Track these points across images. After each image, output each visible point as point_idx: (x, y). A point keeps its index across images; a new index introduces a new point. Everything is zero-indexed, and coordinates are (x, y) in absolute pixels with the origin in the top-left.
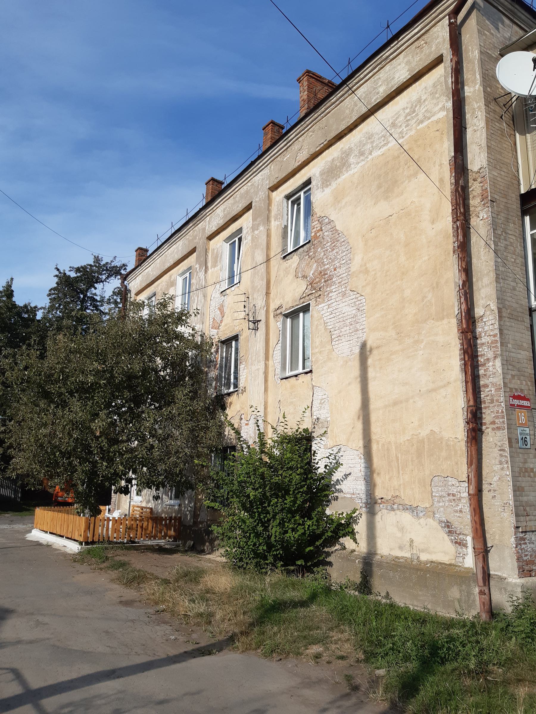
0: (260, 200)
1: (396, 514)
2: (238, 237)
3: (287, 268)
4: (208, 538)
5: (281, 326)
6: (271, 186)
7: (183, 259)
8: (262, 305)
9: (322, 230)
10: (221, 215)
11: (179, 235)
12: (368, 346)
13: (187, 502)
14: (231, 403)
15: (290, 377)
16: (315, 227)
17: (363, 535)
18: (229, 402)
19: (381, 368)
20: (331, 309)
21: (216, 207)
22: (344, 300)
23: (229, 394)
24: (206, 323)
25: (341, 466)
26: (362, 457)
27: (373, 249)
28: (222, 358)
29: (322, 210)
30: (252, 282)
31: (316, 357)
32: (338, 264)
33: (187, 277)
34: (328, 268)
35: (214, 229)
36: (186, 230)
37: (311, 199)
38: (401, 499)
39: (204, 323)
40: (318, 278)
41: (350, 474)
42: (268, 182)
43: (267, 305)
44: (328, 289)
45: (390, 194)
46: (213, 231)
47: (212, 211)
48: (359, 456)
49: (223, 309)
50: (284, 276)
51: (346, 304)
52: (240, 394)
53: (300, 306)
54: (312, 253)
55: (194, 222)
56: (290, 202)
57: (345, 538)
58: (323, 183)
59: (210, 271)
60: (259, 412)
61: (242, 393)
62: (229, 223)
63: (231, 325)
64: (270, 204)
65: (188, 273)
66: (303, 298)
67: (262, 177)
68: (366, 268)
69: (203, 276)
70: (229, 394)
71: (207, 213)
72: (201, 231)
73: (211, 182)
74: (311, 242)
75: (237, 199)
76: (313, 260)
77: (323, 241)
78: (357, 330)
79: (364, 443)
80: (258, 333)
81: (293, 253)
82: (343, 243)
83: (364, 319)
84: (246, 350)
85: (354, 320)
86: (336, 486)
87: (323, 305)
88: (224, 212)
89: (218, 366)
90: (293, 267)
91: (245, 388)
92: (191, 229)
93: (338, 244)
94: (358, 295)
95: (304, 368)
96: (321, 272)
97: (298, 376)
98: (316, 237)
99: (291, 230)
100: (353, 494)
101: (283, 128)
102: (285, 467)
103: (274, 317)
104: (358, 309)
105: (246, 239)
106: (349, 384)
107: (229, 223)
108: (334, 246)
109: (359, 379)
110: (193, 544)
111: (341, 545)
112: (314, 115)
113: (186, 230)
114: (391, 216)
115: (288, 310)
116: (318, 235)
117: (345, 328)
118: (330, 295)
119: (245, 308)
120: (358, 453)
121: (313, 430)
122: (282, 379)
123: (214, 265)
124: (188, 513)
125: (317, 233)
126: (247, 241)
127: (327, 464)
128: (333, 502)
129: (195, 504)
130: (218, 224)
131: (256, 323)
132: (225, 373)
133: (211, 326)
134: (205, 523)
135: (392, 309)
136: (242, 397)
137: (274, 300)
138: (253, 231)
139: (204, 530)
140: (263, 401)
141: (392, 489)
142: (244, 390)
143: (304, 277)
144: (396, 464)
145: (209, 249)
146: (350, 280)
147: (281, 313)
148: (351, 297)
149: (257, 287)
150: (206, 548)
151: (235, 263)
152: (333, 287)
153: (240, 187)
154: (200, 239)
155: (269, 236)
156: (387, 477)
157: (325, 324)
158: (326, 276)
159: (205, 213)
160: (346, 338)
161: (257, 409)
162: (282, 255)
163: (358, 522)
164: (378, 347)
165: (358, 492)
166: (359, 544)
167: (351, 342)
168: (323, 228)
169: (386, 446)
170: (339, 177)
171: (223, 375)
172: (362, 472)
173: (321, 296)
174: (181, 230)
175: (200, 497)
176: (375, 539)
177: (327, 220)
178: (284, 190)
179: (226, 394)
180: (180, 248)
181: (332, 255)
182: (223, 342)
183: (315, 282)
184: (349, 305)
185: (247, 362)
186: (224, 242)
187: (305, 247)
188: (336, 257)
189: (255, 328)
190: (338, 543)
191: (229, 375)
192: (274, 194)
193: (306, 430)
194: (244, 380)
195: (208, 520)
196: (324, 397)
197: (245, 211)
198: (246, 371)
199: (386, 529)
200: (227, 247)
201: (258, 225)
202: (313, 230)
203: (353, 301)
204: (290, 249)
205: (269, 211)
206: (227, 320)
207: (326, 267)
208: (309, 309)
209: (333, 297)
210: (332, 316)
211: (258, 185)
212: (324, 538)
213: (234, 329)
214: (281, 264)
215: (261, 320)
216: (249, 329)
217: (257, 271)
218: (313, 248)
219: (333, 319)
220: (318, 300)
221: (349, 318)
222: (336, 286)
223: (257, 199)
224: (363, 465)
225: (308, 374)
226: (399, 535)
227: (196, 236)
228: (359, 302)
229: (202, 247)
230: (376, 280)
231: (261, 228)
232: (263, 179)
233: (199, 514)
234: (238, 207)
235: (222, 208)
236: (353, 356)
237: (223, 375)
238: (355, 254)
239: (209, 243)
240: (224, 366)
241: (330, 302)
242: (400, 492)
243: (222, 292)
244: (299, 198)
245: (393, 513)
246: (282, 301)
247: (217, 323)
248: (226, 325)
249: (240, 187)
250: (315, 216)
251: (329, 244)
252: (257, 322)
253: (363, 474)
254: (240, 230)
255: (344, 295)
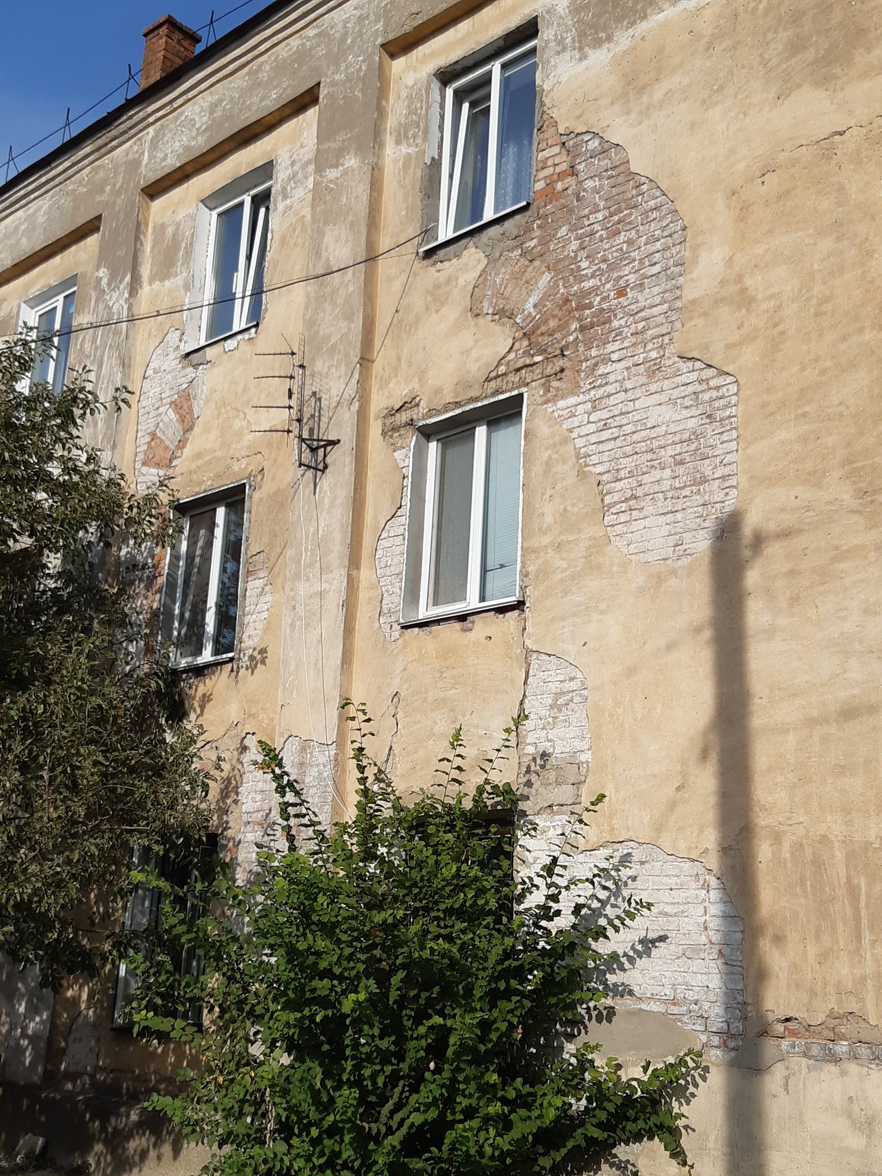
0: (349, 79)
1: (844, 1073)
2: (253, 192)
3: (438, 286)
4: (104, 1129)
5: (410, 462)
6: (391, 37)
7: (48, 251)
8: (346, 395)
9: (573, 174)
10: (202, 121)
11: (43, 179)
12: (747, 531)
13: (22, 1009)
14: (206, 699)
15: (438, 621)
16: (550, 163)
17: (712, 1138)
18: (199, 694)
19: (795, 600)
20: (604, 414)
21: (185, 97)
22: (653, 387)
23: (200, 671)
24: (123, 448)
25: (645, 912)
26: (713, 882)
27: (770, 232)
28: (176, 557)
29: (577, 113)
30: (310, 323)
31: (541, 560)
32: (632, 278)
33: (55, 308)
34: (595, 290)
35: (172, 162)
36: (67, 164)
37: (538, 82)
38: (863, 1025)
39: (119, 448)
40: (554, 317)
41: (663, 939)
42: (380, 26)
43: (363, 395)
44: (594, 352)
45: (838, 70)
46: (167, 170)
47: (168, 109)
48: (702, 878)
49: (190, 408)
50: (427, 309)
51: (663, 397)
52: (242, 671)
53: (486, 402)
54: (535, 241)
55: (100, 142)
56: (449, 92)
57: (635, 1147)
58: (582, 35)
59: (146, 290)
60: (369, 720)
61: (252, 668)
62: (227, 147)
63: (218, 454)
64: (382, 92)
65: (61, 297)
66: (496, 378)
67: (358, 13)
68: (744, 290)
69: (122, 302)
70: (200, 671)
71: (149, 115)
72: (123, 169)
73: (163, 30)
74: (533, 208)
75: (264, 76)
76: (537, 263)
77: (578, 207)
78: (704, 480)
79: (724, 837)
80: (326, 482)
81: (463, 242)
82: (655, 214)
83: (733, 445)
84: (274, 535)
85: (693, 447)
86: (608, 976)
87: (572, 400)
88: (211, 113)
89: (162, 580)
90: (461, 282)
91: (263, 651)
92: (86, 162)
93: (636, 216)
94: (711, 372)
95: (482, 599)
96: (567, 301)
97: (470, 618)
98: (550, 193)
99: (451, 176)
100: (674, 1002)
101: (197, 40)
102: (442, 906)
103: (384, 434)
104: (709, 416)
105: (285, 197)
106: (670, 647)
107: (227, 147)
108: (619, 222)
109: (707, 634)
110: (45, 1148)
111: (618, 1168)
112: (40, 177)
113: (67, 164)
114: (841, 134)
115: (439, 412)
116: (559, 186)
117: (657, 474)
118: (602, 370)
119: (290, 397)
120: (698, 868)
121: (526, 791)
122: (405, 627)
123: (165, 270)
124: (25, 1043)
125: (557, 181)
126: (288, 201)
127: (582, 901)
128: (592, 1025)
129: (54, 1015)
130: (187, 149)
131: (321, 452)
132: (183, 604)
133: (141, 457)
134: (87, 1079)
135: (841, 416)
136: (252, 681)
137: (384, 383)
138: (319, 170)
139: (86, 1101)
140: (336, 693)
141: (831, 989)
142: (260, 657)
143: (504, 314)
144: (849, 911)
145: (147, 225)
146: (678, 325)
147: (411, 423)
148: (684, 379)
149: (328, 338)
150: (91, 1161)
151: (237, 270)
152: (610, 348)
153: (275, 39)
154: (117, 193)
155: (376, 186)
156: (812, 951)
157: (578, 457)
158: (588, 312)
159: (141, 115)
160: (660, 504)
161: (364, 712)
162: (420, 245)
163: (693, 1095)
164: (785, 534)
165: (691, 996)
166: (692, 1167)
167: (679, 516)
168: (581, 167)
169: (808, 852)
170: (644, 17)
171: (177, 612)
172: (712, 933)
173: (567, 372)
174: (49, 164)
175: (70, 993)
176: (760, 1151)
177: (594, 144)
178: (434, 54)
179: (186, 671)
180: (41, 220)
181: (610, 249)
182: (182, 509)
183: (543, 329)
184: (672, 402)
185: (276, 569)
186: (201, 205)
187: (508, 224)
188: (624, 256)
189: (313, 465)
190: (607, 1162)
191: (199, 610)
192: (398, 65)
193: (507, 790)
194: (260, 626)
195: (96, 1068)
196: (568, 686)
197: (288, 111)
198: (268, 598)
199: (802, 1122)
200: (209, 222)
201: (340, 153)
202: (541, 175)
203: (690, 389)
204: (446, 232)
205: (381, 112)
206: (197, 442)
207: (587, 284)
208: (520, 413)
209: (612, 378)
210: (606, 435)
211: (345, 36)
212: (570, 1144)
213: (228, 467)
214: (416, 274)
215: (339, 441)
216: (301, 465)
217: (329, 289)
218: (539, 227)
219: (611, 445)
220: (555, 384)
221: (674, 443)
222: (626, 344)
223: (337, 77)
224: (715, 909)
225: (509, 615)
226: (855, 1141)
227: (104, 182)
228: (714, 394)
229: (122, 215)
230: (781, 328)
231: (351, 162)
232: (361, 19)
233: (64, 1050)
234: (262, 99)
235: (204, 101)
236: (686, 561)
237: (177, 612)
238: (698, 246)
239: (148, 208)
240: (180, 581)
241: (600, 392)
242: (861, 1000)
243: (188, 355)
244: (486, 81)
245: (832, 1068)
246: (415, 384)
247: (166, 448)
248: (199, 455)
249: (275, 39)
250: (550, 132)
251: (600, 216)
252: (325, 446)
253: (714, 939)
254: (266, 170)
255: (654, 370)
